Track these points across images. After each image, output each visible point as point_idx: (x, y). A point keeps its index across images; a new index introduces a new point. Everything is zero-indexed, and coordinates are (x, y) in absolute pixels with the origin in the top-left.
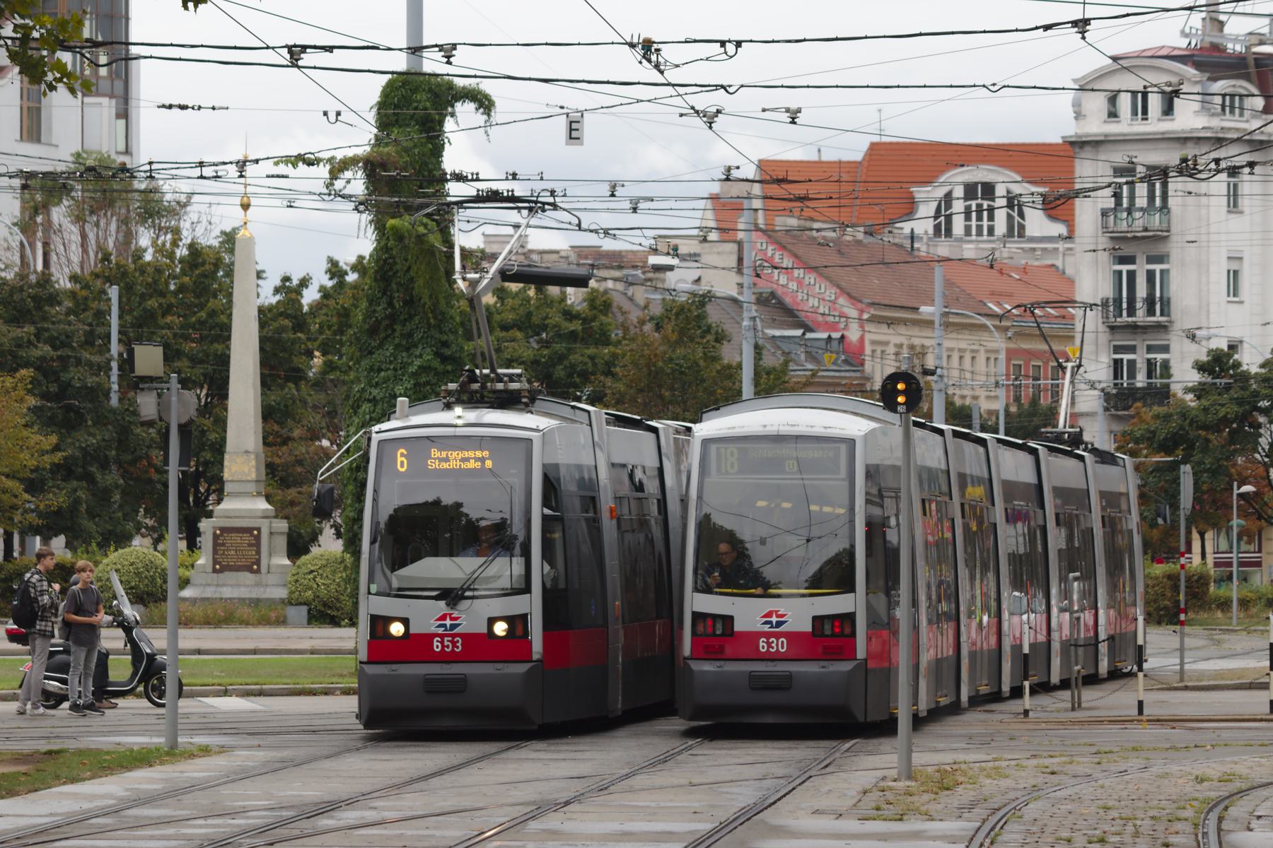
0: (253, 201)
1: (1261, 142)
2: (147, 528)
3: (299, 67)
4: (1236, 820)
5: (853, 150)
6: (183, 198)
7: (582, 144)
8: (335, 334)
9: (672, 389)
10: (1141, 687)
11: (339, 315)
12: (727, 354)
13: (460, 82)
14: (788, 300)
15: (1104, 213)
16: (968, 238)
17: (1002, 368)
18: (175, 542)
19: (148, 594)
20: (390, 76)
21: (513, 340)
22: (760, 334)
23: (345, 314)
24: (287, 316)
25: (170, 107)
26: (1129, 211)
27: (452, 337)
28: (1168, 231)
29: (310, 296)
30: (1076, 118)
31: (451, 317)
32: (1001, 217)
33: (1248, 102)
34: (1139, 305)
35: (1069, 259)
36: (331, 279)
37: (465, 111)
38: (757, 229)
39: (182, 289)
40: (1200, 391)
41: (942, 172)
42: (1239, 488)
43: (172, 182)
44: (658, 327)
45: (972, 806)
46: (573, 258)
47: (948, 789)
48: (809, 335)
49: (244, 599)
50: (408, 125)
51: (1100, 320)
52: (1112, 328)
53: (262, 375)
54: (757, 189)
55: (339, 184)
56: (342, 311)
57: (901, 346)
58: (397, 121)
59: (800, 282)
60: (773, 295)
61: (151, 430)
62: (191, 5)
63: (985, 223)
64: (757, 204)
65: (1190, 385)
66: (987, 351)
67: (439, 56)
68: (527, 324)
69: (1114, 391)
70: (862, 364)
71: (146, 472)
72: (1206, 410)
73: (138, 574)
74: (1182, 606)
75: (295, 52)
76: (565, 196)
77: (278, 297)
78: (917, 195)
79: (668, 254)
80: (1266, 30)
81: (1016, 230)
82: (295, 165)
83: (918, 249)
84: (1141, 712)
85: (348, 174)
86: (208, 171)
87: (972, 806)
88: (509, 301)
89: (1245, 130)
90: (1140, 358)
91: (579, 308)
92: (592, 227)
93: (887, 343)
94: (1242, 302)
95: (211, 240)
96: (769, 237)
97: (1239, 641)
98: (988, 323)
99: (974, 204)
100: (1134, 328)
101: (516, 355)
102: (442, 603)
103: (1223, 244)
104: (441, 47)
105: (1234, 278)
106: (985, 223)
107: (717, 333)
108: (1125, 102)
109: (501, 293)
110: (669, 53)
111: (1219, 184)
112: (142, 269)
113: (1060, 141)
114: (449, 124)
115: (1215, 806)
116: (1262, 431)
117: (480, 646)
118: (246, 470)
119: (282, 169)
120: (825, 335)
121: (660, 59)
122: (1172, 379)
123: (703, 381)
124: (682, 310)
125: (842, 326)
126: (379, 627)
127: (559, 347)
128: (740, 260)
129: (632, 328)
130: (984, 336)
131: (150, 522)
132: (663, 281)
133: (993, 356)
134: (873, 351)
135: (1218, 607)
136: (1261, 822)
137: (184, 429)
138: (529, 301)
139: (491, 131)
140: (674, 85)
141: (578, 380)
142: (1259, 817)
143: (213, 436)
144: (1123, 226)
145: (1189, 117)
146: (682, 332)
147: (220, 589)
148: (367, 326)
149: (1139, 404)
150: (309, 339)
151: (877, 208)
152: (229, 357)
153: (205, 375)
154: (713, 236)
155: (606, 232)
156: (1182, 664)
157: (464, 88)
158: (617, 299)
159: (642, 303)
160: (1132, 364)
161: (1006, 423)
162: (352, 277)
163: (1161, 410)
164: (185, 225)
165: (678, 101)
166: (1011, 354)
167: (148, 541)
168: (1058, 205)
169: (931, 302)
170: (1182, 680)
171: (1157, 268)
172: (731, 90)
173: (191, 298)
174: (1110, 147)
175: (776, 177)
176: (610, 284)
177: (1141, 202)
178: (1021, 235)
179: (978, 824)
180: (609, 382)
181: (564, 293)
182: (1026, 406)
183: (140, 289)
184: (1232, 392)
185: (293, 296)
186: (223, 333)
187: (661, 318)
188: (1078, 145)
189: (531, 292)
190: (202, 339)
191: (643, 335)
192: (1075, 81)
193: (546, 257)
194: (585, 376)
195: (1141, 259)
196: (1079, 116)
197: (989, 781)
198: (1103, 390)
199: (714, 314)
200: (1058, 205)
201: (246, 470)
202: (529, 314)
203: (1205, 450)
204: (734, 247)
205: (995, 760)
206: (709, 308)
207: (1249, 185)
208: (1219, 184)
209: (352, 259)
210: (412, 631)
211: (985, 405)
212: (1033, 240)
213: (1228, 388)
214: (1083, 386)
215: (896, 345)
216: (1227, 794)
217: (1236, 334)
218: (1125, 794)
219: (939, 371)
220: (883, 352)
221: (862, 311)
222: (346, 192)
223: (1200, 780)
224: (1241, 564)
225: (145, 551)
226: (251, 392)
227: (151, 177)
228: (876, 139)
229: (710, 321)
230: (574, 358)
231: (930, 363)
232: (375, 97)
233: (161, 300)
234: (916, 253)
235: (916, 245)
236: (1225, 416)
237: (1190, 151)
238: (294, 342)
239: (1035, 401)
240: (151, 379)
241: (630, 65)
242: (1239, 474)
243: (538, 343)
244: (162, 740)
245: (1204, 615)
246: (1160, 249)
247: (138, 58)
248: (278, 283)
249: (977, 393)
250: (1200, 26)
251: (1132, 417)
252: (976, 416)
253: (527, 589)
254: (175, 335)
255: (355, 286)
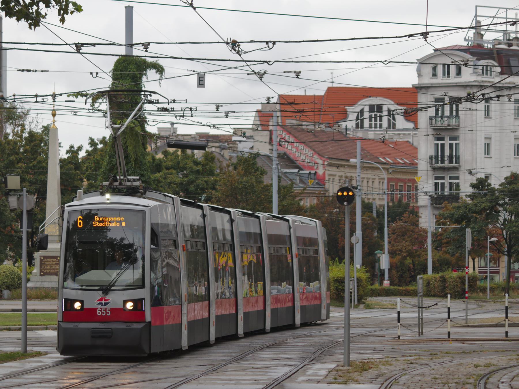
0: (57, 112)
1: (500, 87)
2: (10, 256)
3: (81, 53)
4: (492, 384)
5: (320, 91)
6: (26, 112)
7: (204, 87)
8: (93, 171)
9: (241, 195)
10: (449, 326)
11: (95, 163)
12: (266, 181)
13: (149, 60)
14: (292, 156)
15: (431, 118)
16: (371, 129)
17: (385, 186)
18: (23, 262)
19: (11, 285)
20: (118, 57)
21: (172, 174)
22: (280, 171)
23: (97, 162)
24: (72, 163)
25: (23, 70)
26: (442, 117)
27: (145, 172)
28: (459, 126)
29: (82, 154)
30: (418, 77)
31: (145, 164)
32: (385, 120)
33: (494, 69)
34: (446, 159)
35: (415, 139)
36: (91, 147)
37: (151, 73)
38: (278, 125)
39: (25, 151)
40: (473, 196)
41: (360, 100)
42: (490, 239)
43: (21, 104)
44: (235, 168)
45: (377, 378)
46: (198, 138)
47: (366, 370)
48: (301, 172)
49: (53, 288)
50: (126, 79)
51: (429, 165)
52: (434, 169)
53: (61, 189)
54: (278, 107)
55: (96, 105)
56: (96, 161)
57: (341, 176)
58: (121, 77)
59: (297, 148)
60: (285, 154)
61: (12, 214)
62: (32, 27)
63: (378, 123)
64: (279, 114)
65: (469, 194)
66: (379, 179)
67: (142, 48)
68: (178, 167)
69: (436, 196)
70: (324, 185)
71: (10, 232)
72: (476, 205)
73: (7, 276)
74: (467, 290)
75: (79, 46)
76: (196, 110)
77: (68, 155)
78: (348, 110)
79: (241, 136)
80: (501, 38)
81: (392, 126)
82: (77, 97)
83: (349, 134)
84: (449, 337)
85: (100, 101)
86: (39, 99)
87: (377, 378)
88: (169, 157)
89: (492, 82)
90: (447, 182)
91: (200, 160)
92: (208, 124)
93: (335, 175)
94: (491, 158)
95: (38, 130)
96: (284, 129)
97: (491, 306)
98: (380, 166)
99: (373, 114)
100: (443, 169)
101: (173, 180)
102: (101, 292)
103: (483, 132)
104: (143, 44)
105: (487, 147)
106: (378, 123)
107: (261, 171)
108: (440, 69)
109: (166, 153)
110: (243, 47)
111: (481, 106)
112: (9, 142)
113: (411, 87)
114: (144, 79)
115: (483, 377)
116: (500, 214)
117: (119, 313)
118: (54, 231)
119: (71, 98)
120: (308, 172)
121: (240, 49)
122: (461, 191)
123: (255, 192)
124: (246, 160)
125: (315, 167)
126: (69, 305)
127: (192, 177)
128: (271, 139)
129: (224, 168)
130: (377, 172)
131: (11, 254)
132: (237, 148)
133: (382, 181)
134: (329, 179)
135: (481, 291)
136: (504, 384)
137: (29, 212)
138: (178, 157)
139: (163, 82)
140: (245, 61)
141: (200, 191)
142: (502, 382)
143: (39, 216)
144: (439, 124)
145: (468, 76)
146: (246, 171)
147: (43, 283)
148: (108, 168)
149: (446, 202)
150: (82, 173)
151: (331, 116)
152: (47, 181)
153: (36, 189)
154: (260, 128)
155: (214, 126)
156: (467, 316)
157: (151, 63)
158: (217, 156)
159: (228, 158)
160: (443, 184)
161: (388, 210)
162: (100, 146)
163: (455, 204)
164: (27, 123)
165: (247, 68)
166: (389, 180)
167: (11, 262)
168: (410, 115)
169: (355, 157)
170: (467, 323)
171: (454, 142)
172: (270, 63)
173: (29, 155)
174: (433, 89)
175: (287, 102)
176: (213, 149)
177: (447, 113)
178: (394, 128)
179: (380, 385)
180: (214, 192)
181: (193, 153)
182: (396, 203)
183: (7, 151)
184: (487, 197)
185: (75, 154)
186: (44, 171)
187: (237, 164)
188: (418, 89)
189: (179, 153)
190: (35, 173)
191: (229, 171)
192: (417, 60)
193: (185, 137)
194: (203, 190)
195: (447, 139)
196: (420, 75)
197: (383, 367)
198: (430, 196)
199: (260, 163)
200: (410, 115)
201: (54, 231)
202: (178, 163)
203: (475, 222)
204: (267, 133)
205: (386, 357)
206: (257, 160)
207: (494, 105)
208: (481, 106)
209: (101, 138)
210: (85, 307)
211: (378, 203)
212: (399, 130)
213: (485, 195)
214: (422, 194)
215: (339, 176)
216: (488, 372)
217: (489, 171)
218: (443, 372)
219: (359, 187)
220: (333, 179)
221: (324, 161)
222: (99, 108)
223: (476, 366)
224: (491, 272)
225: (10, 266)
226: (57, 197)
227: (14, 101)
228: (330, 85)
229: (258, 166)
230: (199, 182)
231: (354, 183)
232: (111, 67)
233: (17, 156)
234: (348, 136)
235: (348, 132)
236: (484, 207)
237: (469, 90)
238: (75, 175)
239: (400, 201)
240: (15, 191)
241: (226, 52)
242: (490, 233)
243: (182, 175)
244: (20, 349)
245: (475, 295)
246: (455, 134)
247: (6, 49)
248: (68, 149)
249: (374, 197)
250: (472, 36)
251: (443, 208)
252: (374, 207)
253: (143, 286)
254: (23, 172)
255: (101, 150)
